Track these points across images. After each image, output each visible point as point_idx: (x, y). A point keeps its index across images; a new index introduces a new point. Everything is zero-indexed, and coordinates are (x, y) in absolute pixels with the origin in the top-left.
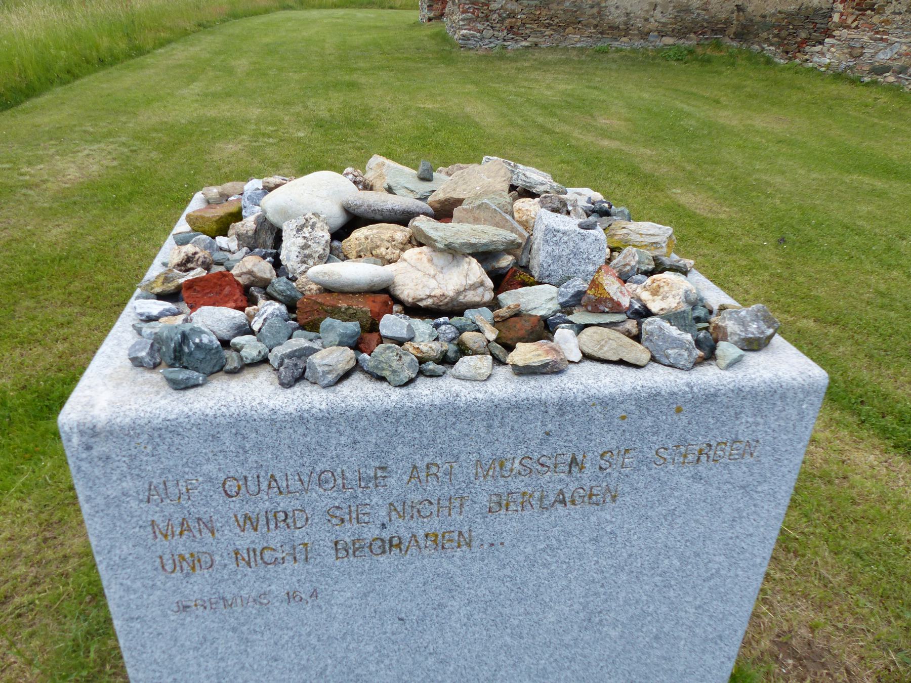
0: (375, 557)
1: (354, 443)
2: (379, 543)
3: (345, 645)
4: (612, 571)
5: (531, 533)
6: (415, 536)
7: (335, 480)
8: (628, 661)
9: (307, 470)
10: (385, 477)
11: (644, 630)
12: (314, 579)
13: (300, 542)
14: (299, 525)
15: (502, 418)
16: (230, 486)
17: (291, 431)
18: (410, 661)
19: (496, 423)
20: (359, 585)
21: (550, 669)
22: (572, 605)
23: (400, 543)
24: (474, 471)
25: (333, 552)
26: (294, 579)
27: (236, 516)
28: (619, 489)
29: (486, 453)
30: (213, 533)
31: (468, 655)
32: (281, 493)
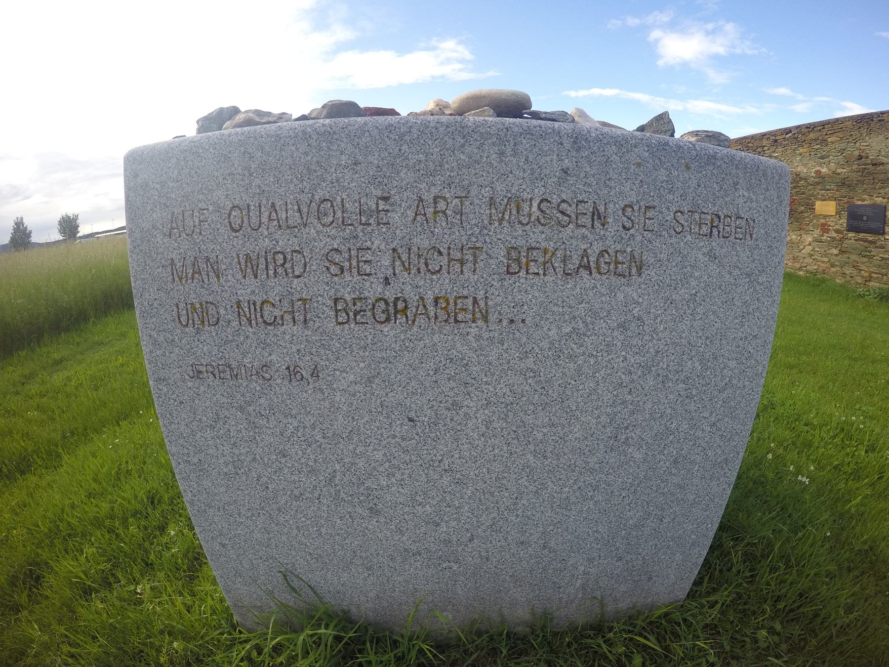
0: (378, 326)
1: (355, 164)
2: (382, 305)
3: (351, 447)
4: (640, 373)
5: (555, 309)
6: (422, 298)
7: (334, 213)
8: (648, 491)
9: (305, 198)
10: (387, 211)
11: (665, 452)
12: (314, 350)
13: (298, 297)
14: (297, 273)
15: (515, 145)
16: (235, 216)
17: (294, 148)
18: (424, 478)
19: (509, 151)
20: (362, 365)
21: (573, 499)
22: (599, 417)
23: (406, 307)
24: (488, 212)
25: (333, 313)
26: (294, 349)
27: (238, 255)
28: (644, 258)
29: (499, 187)
30: (218, 277)
31: (488, 476)
32: (280, 226)
